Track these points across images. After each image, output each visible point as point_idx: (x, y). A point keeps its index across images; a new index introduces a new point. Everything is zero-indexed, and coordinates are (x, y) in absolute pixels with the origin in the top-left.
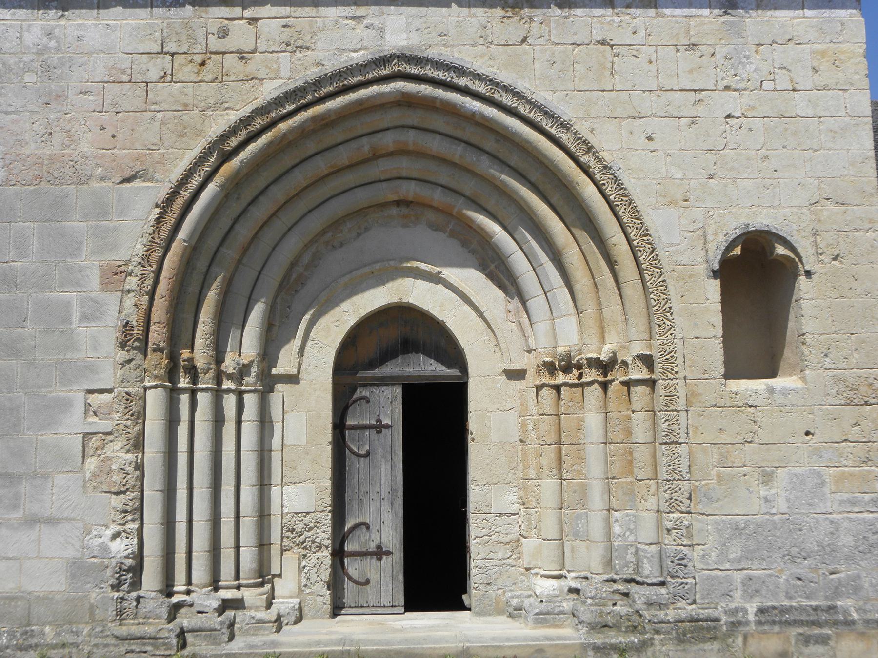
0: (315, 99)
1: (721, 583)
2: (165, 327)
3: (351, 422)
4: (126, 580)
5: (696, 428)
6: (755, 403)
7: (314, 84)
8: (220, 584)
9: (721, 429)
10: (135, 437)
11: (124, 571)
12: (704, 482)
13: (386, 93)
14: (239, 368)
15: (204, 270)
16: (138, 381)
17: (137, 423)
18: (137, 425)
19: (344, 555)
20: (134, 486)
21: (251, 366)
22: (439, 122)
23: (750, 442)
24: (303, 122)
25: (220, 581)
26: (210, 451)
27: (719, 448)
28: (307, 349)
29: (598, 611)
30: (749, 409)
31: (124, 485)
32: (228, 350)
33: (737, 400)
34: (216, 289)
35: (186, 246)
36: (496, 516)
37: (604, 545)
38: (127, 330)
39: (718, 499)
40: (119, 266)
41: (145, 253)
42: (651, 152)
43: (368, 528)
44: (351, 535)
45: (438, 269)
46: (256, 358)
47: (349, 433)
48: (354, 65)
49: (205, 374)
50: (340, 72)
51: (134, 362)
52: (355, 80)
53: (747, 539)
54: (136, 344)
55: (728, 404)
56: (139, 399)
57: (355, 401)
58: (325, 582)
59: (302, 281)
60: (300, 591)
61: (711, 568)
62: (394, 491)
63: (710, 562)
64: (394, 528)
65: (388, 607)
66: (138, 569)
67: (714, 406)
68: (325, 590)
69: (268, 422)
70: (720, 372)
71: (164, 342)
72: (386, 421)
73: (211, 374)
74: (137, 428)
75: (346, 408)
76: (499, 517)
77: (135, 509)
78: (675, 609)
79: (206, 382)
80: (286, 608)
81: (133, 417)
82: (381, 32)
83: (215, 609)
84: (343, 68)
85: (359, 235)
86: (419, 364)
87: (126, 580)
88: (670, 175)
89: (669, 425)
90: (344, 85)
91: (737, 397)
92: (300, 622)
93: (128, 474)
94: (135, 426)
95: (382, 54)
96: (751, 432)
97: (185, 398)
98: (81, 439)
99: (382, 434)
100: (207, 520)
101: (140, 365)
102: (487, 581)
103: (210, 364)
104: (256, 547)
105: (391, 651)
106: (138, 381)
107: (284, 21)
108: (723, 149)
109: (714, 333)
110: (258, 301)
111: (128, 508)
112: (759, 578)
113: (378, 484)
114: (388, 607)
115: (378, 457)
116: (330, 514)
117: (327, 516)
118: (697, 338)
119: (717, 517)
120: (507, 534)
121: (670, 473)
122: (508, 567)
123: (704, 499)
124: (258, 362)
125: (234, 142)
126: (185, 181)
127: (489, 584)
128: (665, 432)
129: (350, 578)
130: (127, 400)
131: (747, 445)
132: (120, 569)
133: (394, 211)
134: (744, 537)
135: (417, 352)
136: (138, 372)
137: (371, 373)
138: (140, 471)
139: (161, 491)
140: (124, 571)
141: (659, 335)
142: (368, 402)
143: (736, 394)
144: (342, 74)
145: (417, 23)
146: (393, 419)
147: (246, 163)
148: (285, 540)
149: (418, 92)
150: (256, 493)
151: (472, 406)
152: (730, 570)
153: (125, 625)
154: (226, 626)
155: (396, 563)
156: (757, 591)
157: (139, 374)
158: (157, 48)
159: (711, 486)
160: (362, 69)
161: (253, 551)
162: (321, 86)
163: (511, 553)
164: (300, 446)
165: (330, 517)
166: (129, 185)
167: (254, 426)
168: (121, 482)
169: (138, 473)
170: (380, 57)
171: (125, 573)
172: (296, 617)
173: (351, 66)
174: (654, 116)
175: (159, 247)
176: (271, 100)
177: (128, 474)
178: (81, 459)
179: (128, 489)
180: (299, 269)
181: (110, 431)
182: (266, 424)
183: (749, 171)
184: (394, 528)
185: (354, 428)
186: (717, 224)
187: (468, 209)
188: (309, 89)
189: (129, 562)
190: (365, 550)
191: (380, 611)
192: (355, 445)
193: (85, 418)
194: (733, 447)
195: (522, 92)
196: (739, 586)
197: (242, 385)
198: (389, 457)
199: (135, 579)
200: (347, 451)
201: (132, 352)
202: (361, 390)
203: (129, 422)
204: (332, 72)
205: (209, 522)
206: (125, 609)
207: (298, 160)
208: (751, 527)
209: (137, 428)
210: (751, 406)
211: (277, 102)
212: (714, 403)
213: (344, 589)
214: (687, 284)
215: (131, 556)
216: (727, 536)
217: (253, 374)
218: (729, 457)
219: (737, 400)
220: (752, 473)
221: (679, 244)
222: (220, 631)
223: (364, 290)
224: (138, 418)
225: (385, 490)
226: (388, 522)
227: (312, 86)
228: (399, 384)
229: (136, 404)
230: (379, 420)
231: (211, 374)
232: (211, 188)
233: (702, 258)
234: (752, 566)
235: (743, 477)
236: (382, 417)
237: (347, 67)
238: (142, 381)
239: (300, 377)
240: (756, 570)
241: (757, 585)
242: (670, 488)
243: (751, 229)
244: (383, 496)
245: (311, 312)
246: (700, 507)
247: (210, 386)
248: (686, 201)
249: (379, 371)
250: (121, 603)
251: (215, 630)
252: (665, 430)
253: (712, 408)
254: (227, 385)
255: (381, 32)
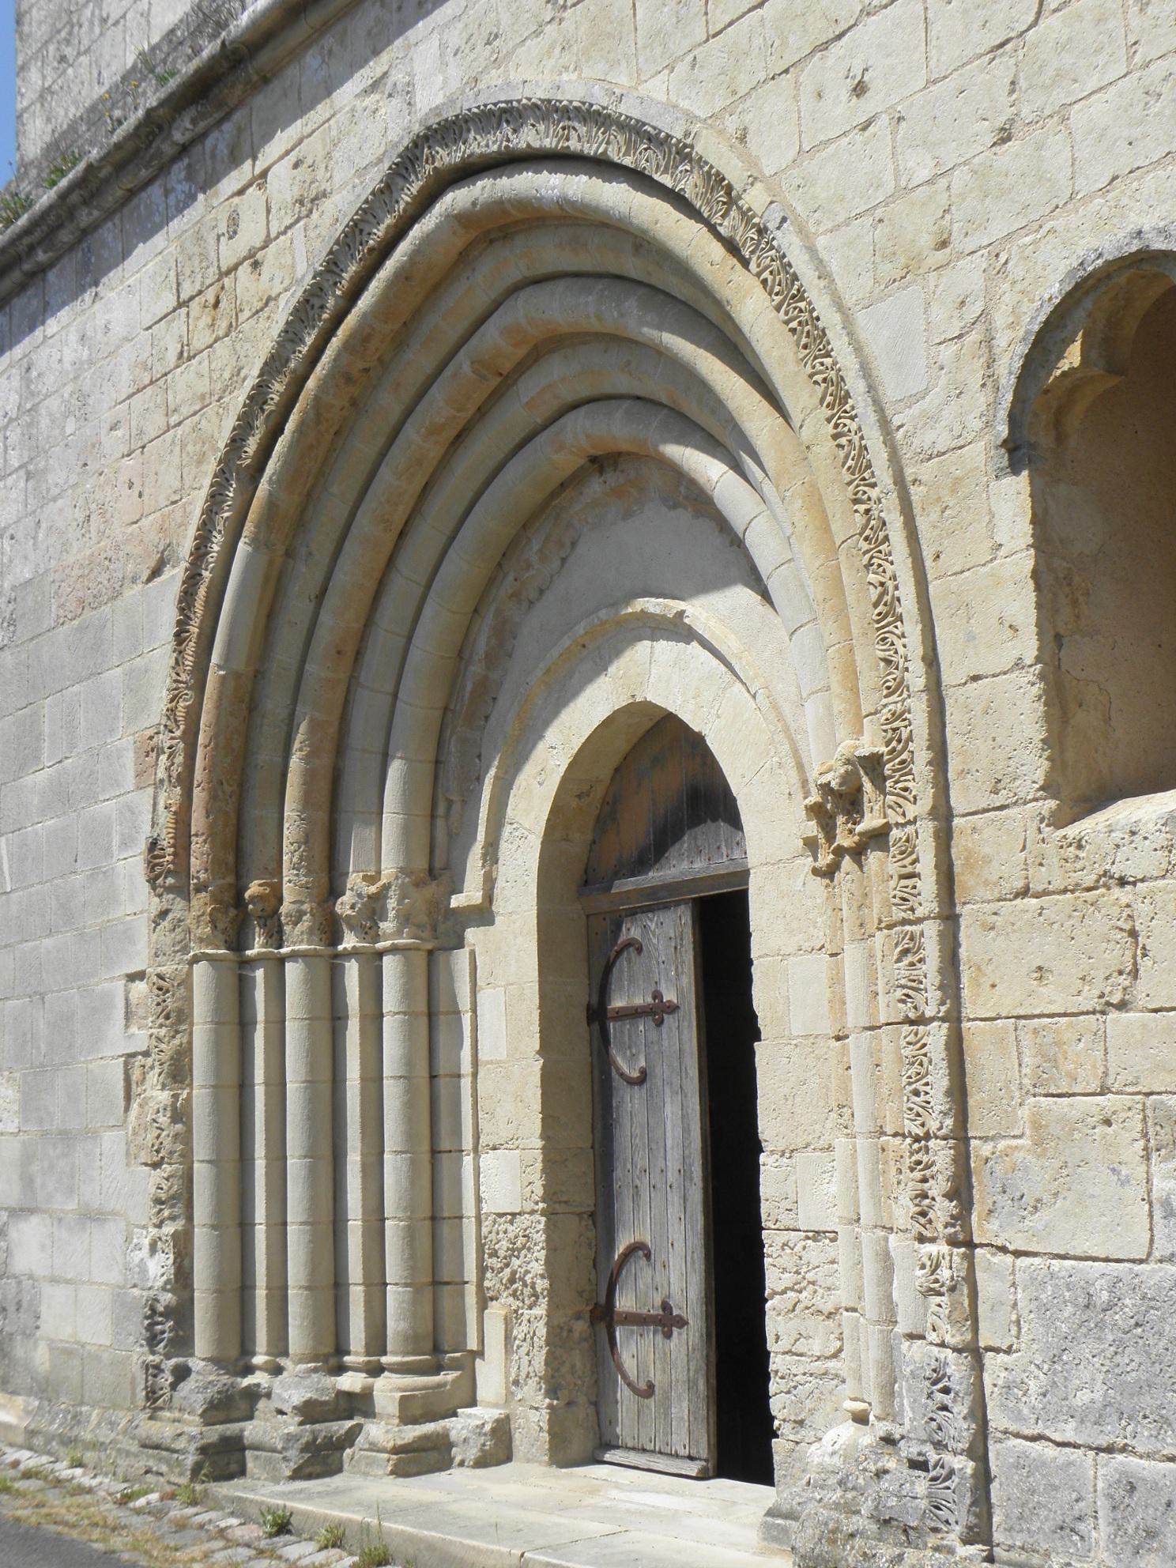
0: (341, 303)
1: (1055, 1488)
2: (205, 841)
3: (618, 1002)
4: (163, 1332)
5: (979, 969)
6: (1131, 871)
7: (328, 270)
8: (347, 1359)
9: (1040, 968)
10: (172, 1058)
11: (161, 1315)
12: (1002, 1144)
13: (433, 231)
14: (363, 904)
15: (284, 714)
16: (178, 951)
17: (177, 1032)
18: (178, 1036)
19: (612, 1319)
20: (171, 1153)
21: (386, 897)
22: (551, 254)
23: (1122, 1006)
24: (335, 360)
25: (348, 1353)
26: (306, 1081)
27: (1035, 1031)
28: (503, 846)
29: (831, 1526)
30: (1117, 892)
31: (158, 1151)
32: (351, 870)
33: (1079, 865)
34: (301, 750)
35: (223, 677)
36: (808, 1238)
37: (882, 1331)
38: (155, 857)
39: (1038, 1200)
40: (151, 738)
41: (169, 706)
42: (864, 129)
43: (648, 1256)
44: (624, 1272)
45: (679, 605)
46: (397, 878)
47: (614, 1028)
48: (370, 197)
49: (296, 924)
50: (356, 225)
51: (170, 916)
52: (380, 231)
53: (1120, 1346)
54: (170, 881)
55: (1058, 884)
56: (179, 985)
57: (619, 953)
58: (540, 1378)
59: (486, 692)
60: (510, 1395)
61: (1027, 1432)
62: (685, 1173)
63: (1026, 1411)
64: (689, 1258)
65: (683, 1457)
66: (182, 1313)
67: (1024, 893)
68: (540, 1397)
69: (448, 1013)
70: (1035, 778)
71: (206, 870)
72: (670, 996)
73: (306, 924)
74: (177, 1042)
75: (608, 969)
76: (815, 1240)
77: (173, 1197)
78: (937, 1549)
79: (298, 939)
80: (462, 1429)
81: (168, 1022)
82: (408, 92)
83: (295, 1408)
84: (357, 214)
85: (564, 560)
86: (719, 848)
87: (163, 1332)
88: (903, 183)
89: (912, 964)
90: (371, 250)
91: (1082, 854)
92: (499, 1463)
93: (163, 1130)
94: (174, 1037)
95: (401, 149)
96: (1121, 973)
97: (352, 972)
98: (122, 1065)
99: (665, 1028)
100: (302, 1223)
101: (180, 921)
102: (796, 1415)
103: (302, 903)
104: (406, 1285)
105: (421, 1540)
106: (178, 951)
107: (292, 158)
108: (1035, 23)
109: (1016, 654)
110: (394, 757)
111: (163, 1196)
112: (1155, 1487)
113: (662, 1150)
114: (683, 1457)
115: (660, 1084)
116: (543, 1219)
117: (539, 1222)
118: (976, 678)
119: (1037, 1260)
120: (829, 1289)
121: (918, 1115)
122: (835, 1382)
123: (1003, 1201)
124: (402, 887)
125: (252, 445)
126: (203, 550)
127: (801, 1423)
128: (903, 987)
129: (625, 1377)
130: (160, 989)
131: (1114, 1015)
132: (153, 1310)
133: (596, 487)
134: (1110, 1338)
135: (714, 820)
136: (179, 934)
137: (633, 883)
138: (183, 1123)
139: (209, 1162)
140: (161, 1315)
141: (885, 692)
142: (640, 950)
143: (1080, 847)
144: (361, 226)
145: (454, 38)
146: (680, 992)
147: (278, 481)
148: (489, 1275)
149: (474, 204)
150: (405, 1168)
151: (758, 947)
152: (1076, 1446)
153: (161, 1420)
154: (298, 1445)
155: (694, 1350)
156: (1151, 1534)
157: (178, 938)
158: (171, 301)
159: (1019, 1156)
160: (386, 197)
161: (399, 1293)
162: (342, 271)
163: (839, 1343)
164: (498, 1062)
165: (542, 1226)
166: (158, 580)
167: (396, 1025)
168: (153, 1146)
169: (179, 1127)
170: (400, 156)
171: (160, 1319)
172: (482, 1450)
173: (366, 201)
174: (868, 14)
175: (187, 688)
176: (280, 336)
177: (163, 1130)
178: (122, 1103)
179: (163, 1158)
180: (476, 669)
181: (145, 1049)
182: (442, 1018)
183: (1101, 60)
184: (689, 1258)
185: (633, 1014)
186: (1019, 287)
187: (679, 441)
188: (326, 285)
189: (167, 1298)
190: (645, 1311)
191: (661, 1463)
192: (624, 1057)
193: (127, 1026)
194: (1071, 1025)
195: (604, 108)
196: (1102, 1504)
197: (377, 938)
198: (676, 1081)
199: (181, 1333)
200: (614, 1070)
201: (166, 897)
202: (629, 925)
203: (163, 1031)
204: (343, 231)
205: (308, 1228)
206: (162, 1389)
207: (381, 441)
208: (1127, 1301)
209: (177, 1042)
210: (1122, 882)
211: (290, 335)
212: (1019, 884)
213: (617, 1402)
214: (948, 512)
215: (168, 1287)
216: (1064, 1328)
217: (391, 914)
218: (1061, 1060)
219: (1079, 865)
220: (1124, 1115)
221: (927, 391)
222: (281, 1453)
223: (575, 693)
224: (179, 1021)
225: (673, 1164)
226: (679, 1246)
227: (328, 276)
228: (685, 902)
229: (173, 995)
230: (657, 995)
231: (306, 924)
232: (243, 548)
233: (982, 415)
234: (1133, 1443)
235: (1101, 1129)
236: (663, 988)
237: (360, 208)
238: (185, 949)
239: (493, 909)
240: (1148, 1456)
241: (1151, 1511)
242: (919, 1163)
243: (1090, 269)
244: (670, 1180)
245: (496, 763)
246: (994, 1225)
247: (303, 947)
248: (944, 244)
249: (655, 876)
250: (155, 1376)
251: (274, 1450)
252: (903, 982)
253: (1019, 901)
254: (349, 942)
255: (408, 92)
